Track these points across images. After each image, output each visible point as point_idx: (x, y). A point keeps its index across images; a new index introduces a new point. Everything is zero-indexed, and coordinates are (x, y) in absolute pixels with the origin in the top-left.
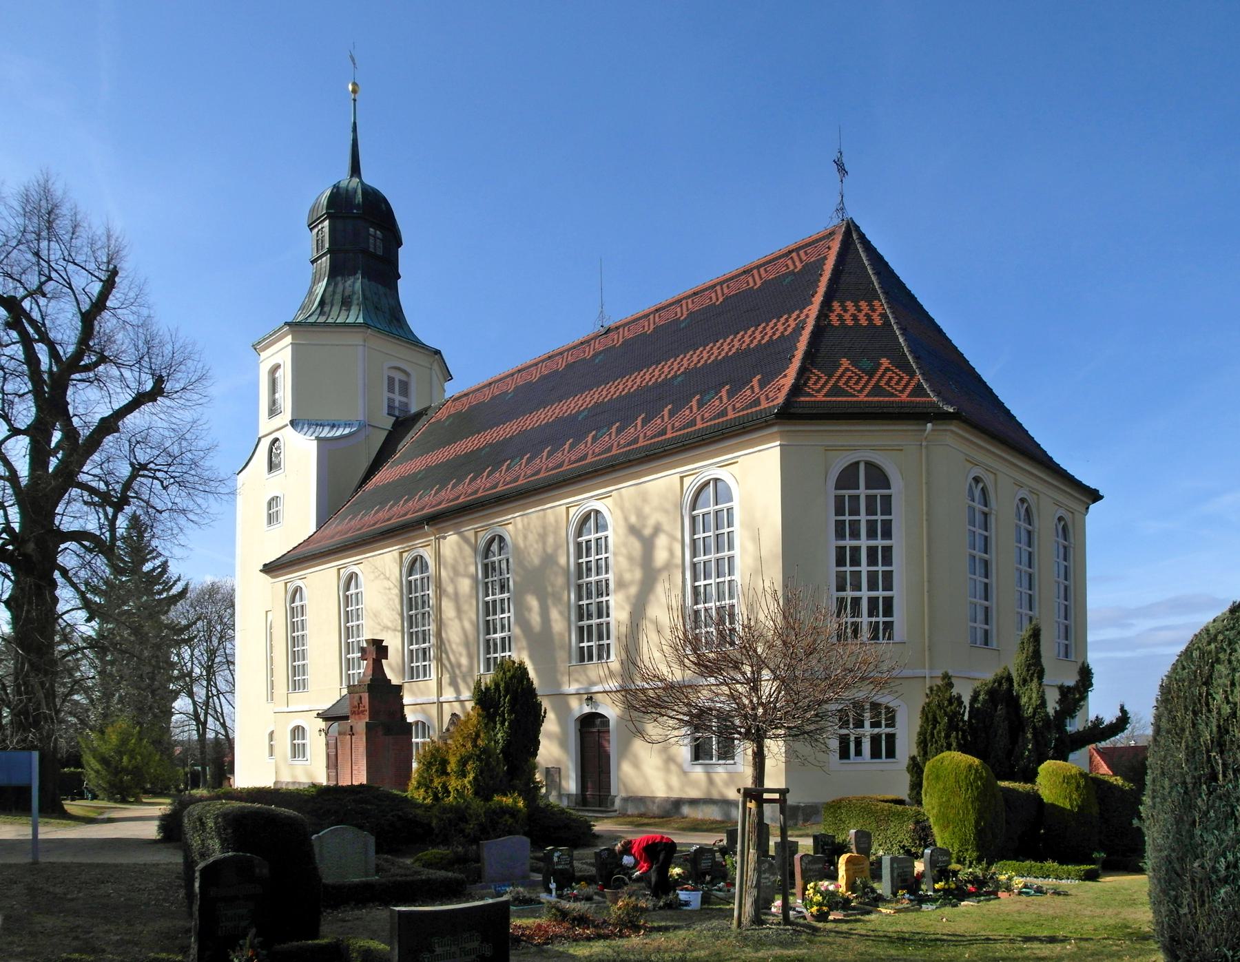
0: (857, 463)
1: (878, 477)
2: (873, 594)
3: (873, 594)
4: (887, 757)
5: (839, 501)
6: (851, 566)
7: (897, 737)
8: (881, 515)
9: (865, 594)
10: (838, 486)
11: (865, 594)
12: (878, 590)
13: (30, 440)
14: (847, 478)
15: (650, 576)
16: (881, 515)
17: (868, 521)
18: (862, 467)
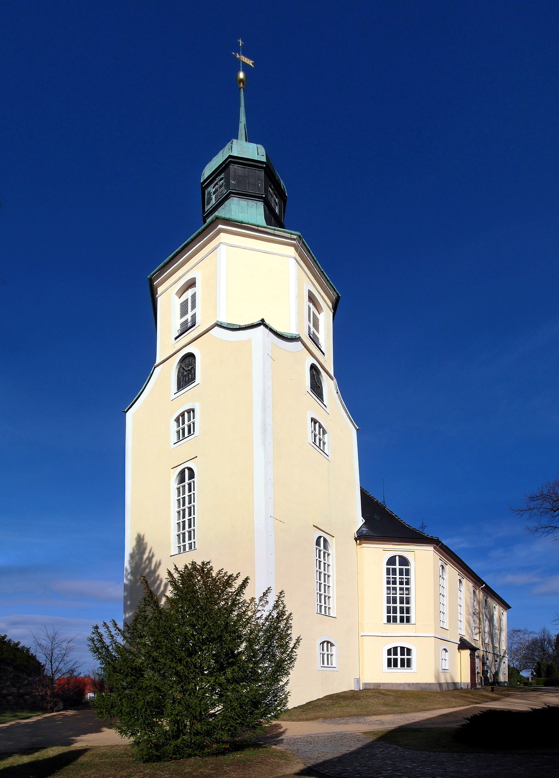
0: (395, 556)
1: (404, 561)
2: (402, 605)
3: (402, 605)
4: (404, 648)
5: (388, 570)
6: (404, 659)
7: (386, 584)
8: (406, 614)
9: (398, 605)
10: (388, 564)
11: (398, 605)
12: (404, 655)
13: (263, 325)
14: (391, 561)
15: (449, 770)
16: (406, 614)
17: (404, 659)
18: (397, 558)
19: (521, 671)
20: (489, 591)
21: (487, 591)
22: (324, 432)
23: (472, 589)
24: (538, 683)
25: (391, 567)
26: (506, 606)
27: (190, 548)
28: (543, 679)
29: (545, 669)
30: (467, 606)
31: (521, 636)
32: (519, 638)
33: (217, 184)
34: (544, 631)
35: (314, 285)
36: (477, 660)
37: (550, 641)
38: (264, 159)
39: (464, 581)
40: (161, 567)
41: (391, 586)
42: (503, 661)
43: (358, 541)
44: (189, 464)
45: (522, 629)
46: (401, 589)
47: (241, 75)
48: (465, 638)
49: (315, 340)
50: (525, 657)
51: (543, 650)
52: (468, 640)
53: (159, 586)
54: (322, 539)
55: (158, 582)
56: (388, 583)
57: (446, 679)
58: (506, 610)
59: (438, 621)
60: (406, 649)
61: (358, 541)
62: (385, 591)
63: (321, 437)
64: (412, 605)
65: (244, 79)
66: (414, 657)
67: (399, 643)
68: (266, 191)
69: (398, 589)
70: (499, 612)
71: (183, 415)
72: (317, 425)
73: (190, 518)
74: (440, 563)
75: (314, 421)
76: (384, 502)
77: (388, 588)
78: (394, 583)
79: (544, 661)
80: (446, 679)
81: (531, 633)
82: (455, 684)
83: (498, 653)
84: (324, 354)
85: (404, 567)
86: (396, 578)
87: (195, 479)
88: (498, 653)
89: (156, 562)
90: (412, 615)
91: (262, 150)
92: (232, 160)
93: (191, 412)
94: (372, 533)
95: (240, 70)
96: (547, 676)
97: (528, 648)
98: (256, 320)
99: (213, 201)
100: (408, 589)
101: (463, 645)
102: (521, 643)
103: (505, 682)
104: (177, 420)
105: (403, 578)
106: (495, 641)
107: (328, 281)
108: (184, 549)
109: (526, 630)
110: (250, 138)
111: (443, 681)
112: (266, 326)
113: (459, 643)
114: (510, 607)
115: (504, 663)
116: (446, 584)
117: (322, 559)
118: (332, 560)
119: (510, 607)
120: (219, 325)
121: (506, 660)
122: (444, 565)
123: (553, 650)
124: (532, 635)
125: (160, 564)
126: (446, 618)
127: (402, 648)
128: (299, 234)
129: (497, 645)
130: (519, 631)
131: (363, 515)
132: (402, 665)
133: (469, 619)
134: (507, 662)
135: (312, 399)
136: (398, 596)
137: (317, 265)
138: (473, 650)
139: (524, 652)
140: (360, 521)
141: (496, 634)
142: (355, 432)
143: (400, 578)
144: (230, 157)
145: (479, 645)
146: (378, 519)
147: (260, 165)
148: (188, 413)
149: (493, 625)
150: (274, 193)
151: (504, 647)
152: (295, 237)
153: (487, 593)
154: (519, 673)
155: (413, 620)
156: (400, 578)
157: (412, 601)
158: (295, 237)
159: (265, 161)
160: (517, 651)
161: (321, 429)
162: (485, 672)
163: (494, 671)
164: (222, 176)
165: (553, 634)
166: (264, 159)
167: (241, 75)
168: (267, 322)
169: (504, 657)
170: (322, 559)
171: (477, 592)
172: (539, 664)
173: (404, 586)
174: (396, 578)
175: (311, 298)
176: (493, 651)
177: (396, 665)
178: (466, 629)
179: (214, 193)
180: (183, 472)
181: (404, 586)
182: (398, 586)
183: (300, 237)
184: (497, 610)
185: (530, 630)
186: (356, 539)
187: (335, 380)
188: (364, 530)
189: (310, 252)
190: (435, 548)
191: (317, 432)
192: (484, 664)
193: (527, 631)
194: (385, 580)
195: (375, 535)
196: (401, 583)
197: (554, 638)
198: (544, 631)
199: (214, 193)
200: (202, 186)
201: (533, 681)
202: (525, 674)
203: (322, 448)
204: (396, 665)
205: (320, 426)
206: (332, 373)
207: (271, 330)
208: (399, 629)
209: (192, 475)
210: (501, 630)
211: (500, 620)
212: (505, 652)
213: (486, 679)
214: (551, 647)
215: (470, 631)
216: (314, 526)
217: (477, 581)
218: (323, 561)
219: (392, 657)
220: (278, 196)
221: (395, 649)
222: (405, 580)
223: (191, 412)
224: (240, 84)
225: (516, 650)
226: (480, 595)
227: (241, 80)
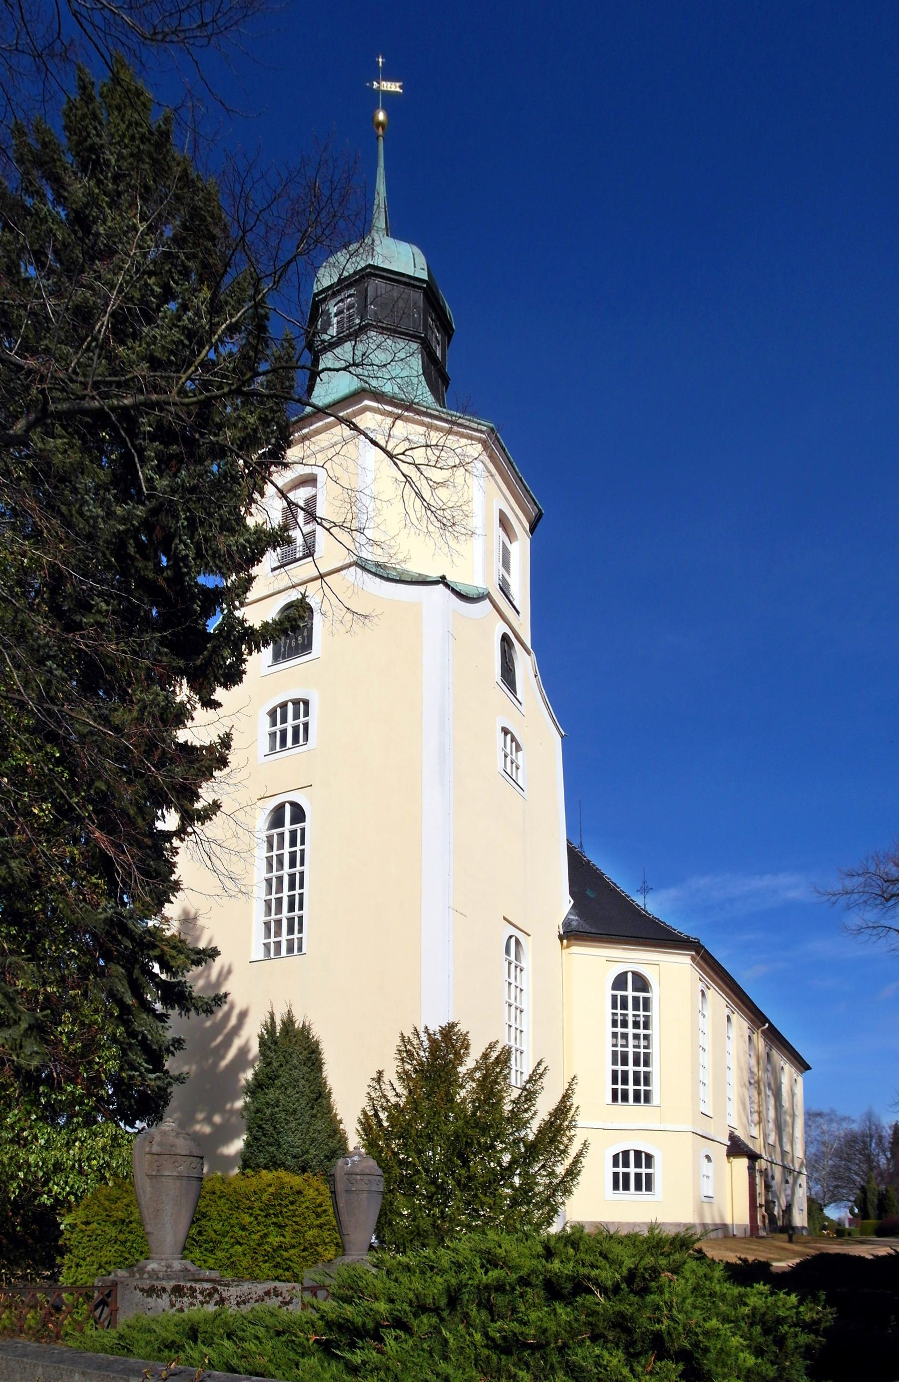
0: (626, 973)
1: (641, 984)
14: (620, 982)
18: (630, 975)
19: (825, 1206)
20: (775, 1037)
21: (771, 1036)
22: (518, 748)
23: (747, 1032)
24: (863, 1233)
25: (619, 993)
26: (803, 1066)
27: (290, 950)
28: (873, 1222)
29: (876, 1201)
30: (740, 1069)
31: (825, 1127)
32: (819, 1131)
33: (342, 301)
34: (869, 1116)
35: (506, 499)
36: (758, 1179)
37: (881, 1138)
38: (424, 276)
39: (735, 1018)
40: (232, 978)
41: (619, 1030)
42: (799, 1181)
43: (565, 941)
44: (299, 798)
45: (826, 1110)
46: (636, 1037)
47: (381, 116)
48: (737, 1133)
49: (504, 589)
50: (835, 1174)
51: (869, 1159)
52: (742, 1138)
53: (228, 1015)
54: (513, 940)
55: (225, 1007)
56: (614, 1024)
57: (713, 1218)
58: (802, 1072)
59: (696, 1098)
60: (643, 1155)
61: (565, 941)
62: (609, 1040)
63: (514, 757)
64: (655, 1069)
65: (386, 123)
66: (658, 1171)
67: (632, 1145)
68: (426, 326)
69: (630, 1037)
70: (791, 1077)
71: (284, 706)
72: (509, 736)
73: (292, 893)
74: (700, 986)
75: (506, 731)
76: (581, 846)
77: (615, 1035)
78: (624, 1024)
79: (873, 1184)
80: (713, 1218)
81: (843, 1119)
82: (725, 1226)
83: (791, 1165)
84: (518, 612)
85: (641, 995)
86: (627, 1015)
87: (307, 824)
88: (791, 1165)
89: (222, 968)
90: (655, 1087)
91: (421, 260)
92: (373, 272)
93: (301, 703)
94: (587, 927)
95: (378, 108)
96: (879, 1217)
97: (838, 1154)
98: (435, 574)
99: (333, 331)
100: (646, 1037)
101: (736, 1148)
102: (824, 1143)
103: (803, 1228)
104: (272, 714)
105: (639, 1016)
106: (785, 1139)
107: (527, 491)
108: (278, 951)
109: (833, 1112)
110: (396, 231)
111: (708, 1221)
112: (447, 585)
113: (729, 1143)
114: (808, 1068)
115: (800, 1186)
116: (706, 1025)
117: (512, 980)
118: (526, 980)
119: (808, 1068)
120: (361, 565)
121: (803, 1180)
122: (706, 990)
123: (888, 1159)
124: (845, 1125)
125: (229, 972)
126: (706, 1093)
127: (638, 1153)
128: (491, 425)
129: (787, 1148)
130: (820, 1115)
131: (572, 893)
132: (638, 1187)
133: (743, 1095)
134: (804, 1185)
135: (501, 692)
136: (631, 1050)
137: (506, 454)
138: (753, 1157)
139: (830, 1162)
140: (565, 903)
141: (785, 1121)
142: (559, 740)
143: (634, 1015)
144: (370, 266)
145: (757, 1147)
146: (592, 896)
147: (418, 284)
148: (293, 704)
149: (781, 1106)
150: (436, 326)
151: (799, 1152)
152: (484, 428)
153: (771, 1040)
154: (822, 1210)
155: (655, 1098)
156: (634, 1015)
157: (655, 1060)
158: (484, 428)
159: (426, 278)
160: (816, 1161)
161: (514, 744)
162: (769, 1205)
163: (783, 1202)
164: (352, 292)
165: (887, 1121)
166: (424, 276)
167: (381, 116)
168: (449, 578)
169: (800, 1173)
170: (512, 980)
171: (755, 1036)
172: (863, 1190)
173: (641, 1031)
174: (627, 1015)
175: (504, 522)
176: (782, 1161)
177: (626, 1187)
178: (739, 1116)
179: (336, 315)
180: (280, 808)
181: (641, 1031)
182: (630, 1031)
183: (492, 429)
184: (788, 1073)
185: (841, 1112)
186: (561, 938)
187: (533, 655)
188: (573, 920)
189: (504, 450)
190: (693, 959)
191: (508, 751)
192: (768, 1187)
193: (836, 1115)
194: (609, 1019)
195: (593, 931)
196: (636, 1025)
197: (888, 1132)
198: (869, 1116)
199: (336, 315)
200: (314, 299)
201: (853, 1228)
202: (835, 1213)
203: (514, 778)
204: (626, 1187)
205: (513, 739)
206: (529, 644)
207: (454, 591)
208: (631, 1112)
209: (299, 815)
210: (793, 1116)
211: (793, 1094)
212: (802, 1162)
213: (772, 1218)
214: (884, 1152)
215: (745, 1120)
216: (505, 919)
217: (756, 1017)
218: (514, 984)
219: (621, 1170)
220: (441, 330)
221: (626, 1153)
222: (642, 1019)
223: (301, 703)
224: (378, 128)
225: (814, 1158)
226: (760, 1042)
227: (379, 124)
